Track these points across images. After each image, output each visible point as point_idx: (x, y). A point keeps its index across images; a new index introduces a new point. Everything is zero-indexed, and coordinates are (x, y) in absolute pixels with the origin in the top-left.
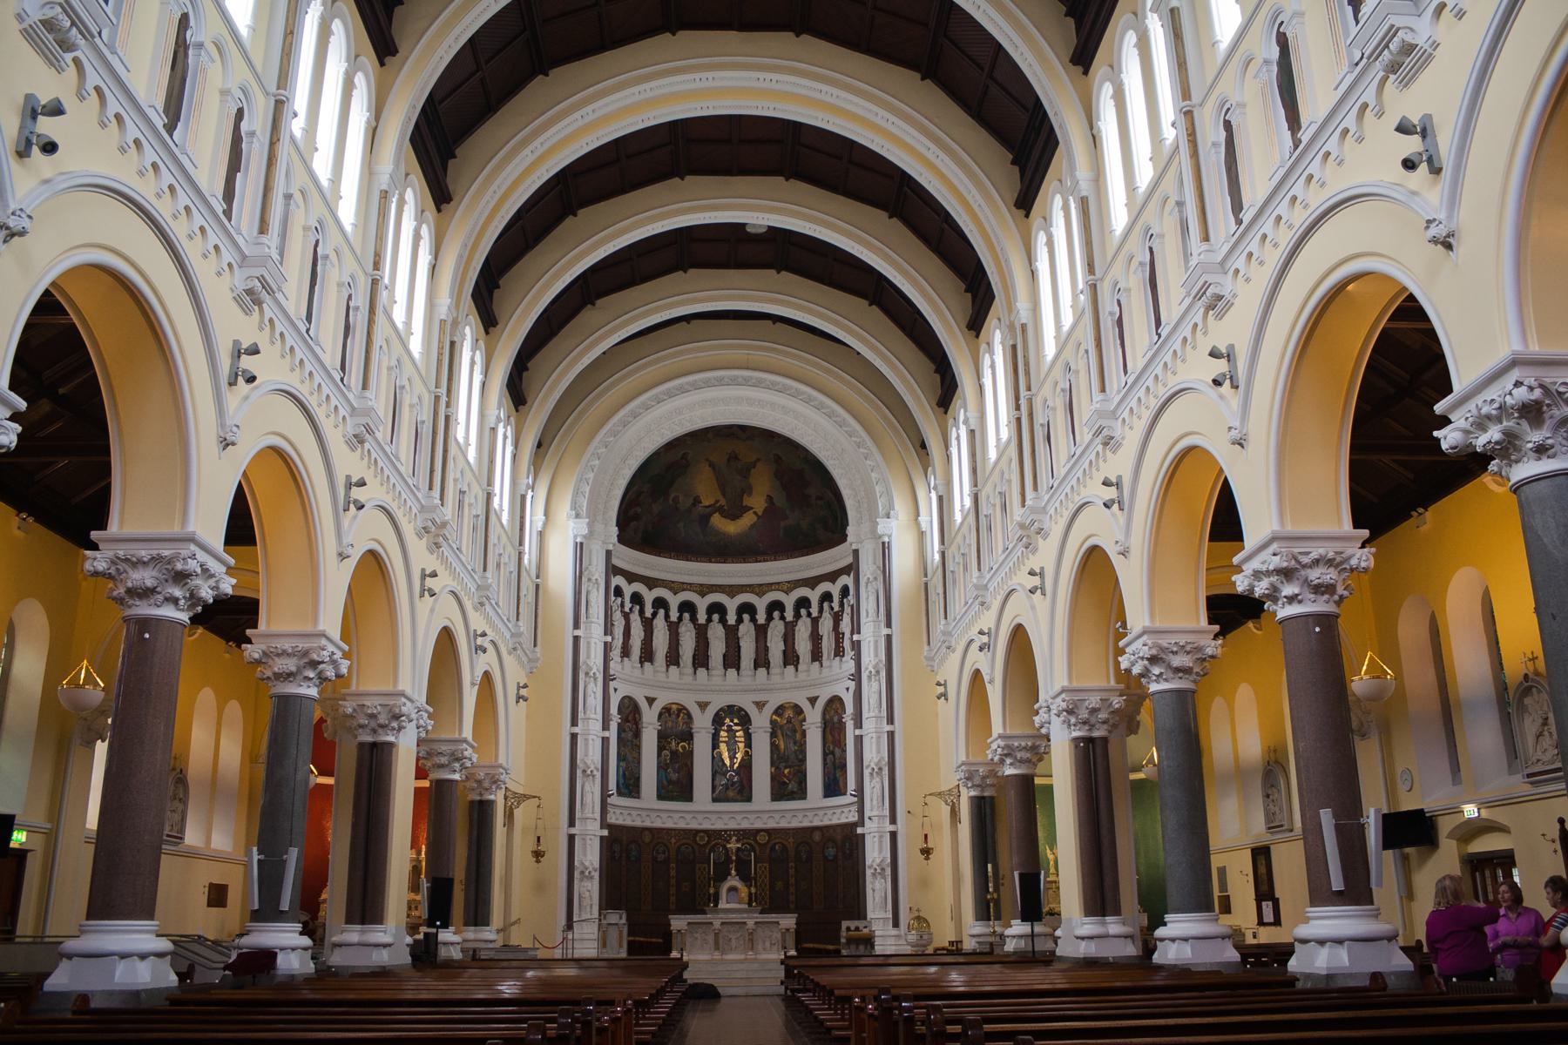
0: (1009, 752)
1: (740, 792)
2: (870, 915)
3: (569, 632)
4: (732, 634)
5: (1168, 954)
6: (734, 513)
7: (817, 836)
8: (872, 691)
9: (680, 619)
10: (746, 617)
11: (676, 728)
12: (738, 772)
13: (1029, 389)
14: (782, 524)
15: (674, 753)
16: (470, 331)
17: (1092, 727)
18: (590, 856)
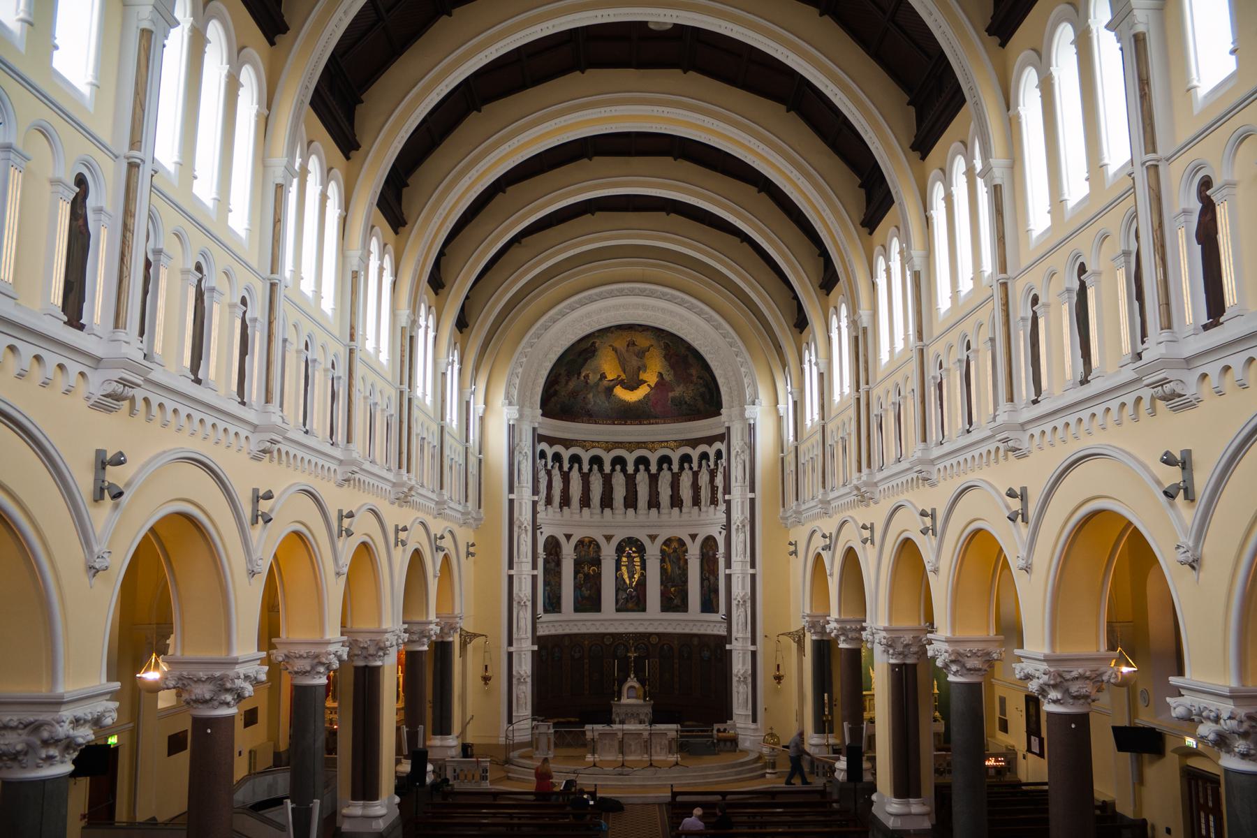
1: (637, 604)
3: (505, 496)
4: (631, 481)
6: (632, 387)
7: (696, 641)
9: (590, 470)
10: (642, 467)
11: (588, 555)
12: (636, 589)
13: (867, 383)
14: (671, 395)
15: (587, 576)
17: (905, 656)
18: (524, 667)
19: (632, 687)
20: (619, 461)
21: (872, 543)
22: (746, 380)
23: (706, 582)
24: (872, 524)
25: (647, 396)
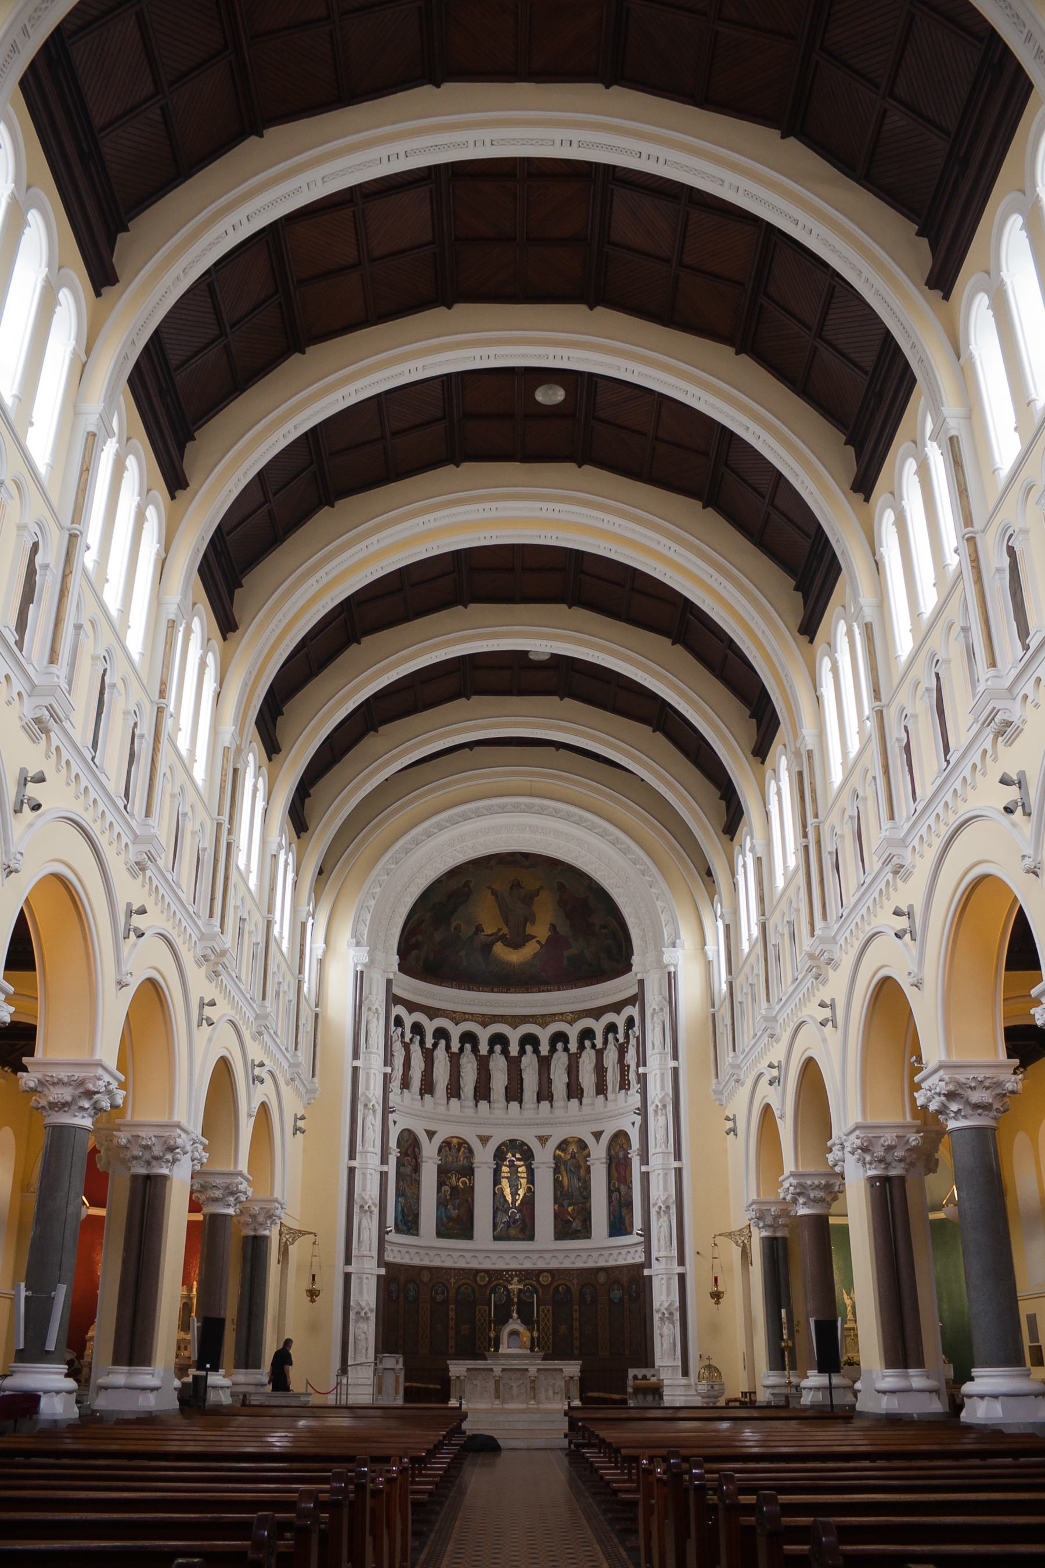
0: (801, 1191)
1: (522, 1230)
2: (658, 1363)
3: (348, 1063)
4: (514, 1067)
5: (978, 1412)
6: (517, 942)
7: (602, 1278)
8: (659, 1125)
9: (461, 1049)
10: (529, 1048)
12: (520, 1209)
13: (816, 816)
14: (566, 953)
15: (454, 1189)
16: (253, 758)
17: (888, 1165)
18: (366, 1296)
19: (514, 1333)
21: (835, 1026)
22: (663, 917)
23: (615, 1195)
24: (833, 1000)
25: (535, 955)
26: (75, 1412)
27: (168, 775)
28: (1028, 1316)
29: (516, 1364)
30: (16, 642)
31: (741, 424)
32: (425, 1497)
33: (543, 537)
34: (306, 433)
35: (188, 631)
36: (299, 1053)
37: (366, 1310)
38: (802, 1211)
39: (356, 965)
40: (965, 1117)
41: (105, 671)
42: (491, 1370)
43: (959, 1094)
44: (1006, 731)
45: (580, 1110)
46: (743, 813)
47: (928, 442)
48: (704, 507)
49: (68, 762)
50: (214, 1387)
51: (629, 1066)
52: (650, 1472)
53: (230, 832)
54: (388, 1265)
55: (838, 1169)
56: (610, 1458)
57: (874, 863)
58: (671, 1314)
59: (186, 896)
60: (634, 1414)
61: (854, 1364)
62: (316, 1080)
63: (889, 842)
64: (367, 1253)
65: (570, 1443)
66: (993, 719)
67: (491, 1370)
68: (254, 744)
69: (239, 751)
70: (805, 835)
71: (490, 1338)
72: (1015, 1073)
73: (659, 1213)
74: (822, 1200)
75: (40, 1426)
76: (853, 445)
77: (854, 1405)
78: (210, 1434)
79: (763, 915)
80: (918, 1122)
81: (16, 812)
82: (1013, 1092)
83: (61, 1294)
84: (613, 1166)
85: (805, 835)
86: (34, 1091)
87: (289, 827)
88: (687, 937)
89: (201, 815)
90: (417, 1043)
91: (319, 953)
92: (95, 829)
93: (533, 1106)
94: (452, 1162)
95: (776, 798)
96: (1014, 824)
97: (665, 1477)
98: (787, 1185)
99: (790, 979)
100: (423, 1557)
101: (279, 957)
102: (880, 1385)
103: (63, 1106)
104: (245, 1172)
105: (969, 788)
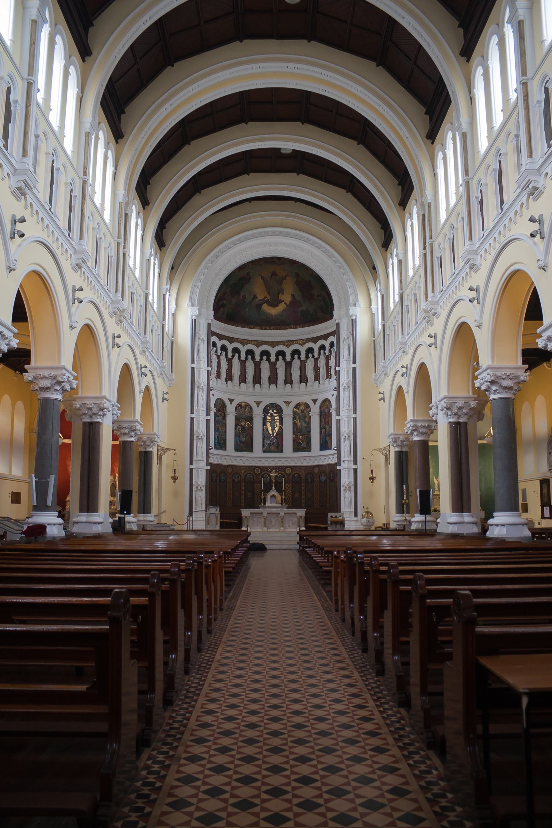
0: (416, 429)
1: (277, 447)
3: (189, 366)
5: (494, 532)
6: (274, 303)
7: (316, 470)
8: (346, 396)
9: (246, 358)
10: (280, 358)
11: (244, 415)
12: (276, 437)
13: (431, 238)
14: (299, 309)
15: (244, 428)
16: (135, 208)
18: (201, 479)
20: (265, 353)
21: (436, 347)
22: (350, 291)
23: (323, 430)
24: (436, 334)
25: (284, 310)
26: (63, 533)
27: (91, 217)
28: (522, 490)
29: (274, 510)
30: (4, 145)
31: (400, 15)
32: (231, 569)
33: (288, 83)
34: (156, 22)
35: (97, 139)
36: (164, 361)
37: (201, 486)
38: (416, 438)
39: (192, 316)
40: (499, 393)
41: (53, 161)
42: (262, 513)
43: (497, 382)
44: (534, 192)
45: (306, 388)
46: (392, 236)
47: (506, 24)
48: (377, 66)
49: (37, 211)
50: (129, 522)
51: (331, 367)
52: (337, 557)
53: (124, 247)
54: (211, 465)
55: (434, 418)
56: (319, 553)
57: (460, 263)
58: (350, 487)
59: (103, 281)
60: (331, 533)
61: (437, 511)
62: (173, 374)
63: (469, 252)
64: (201, 459)
65: (300, 546)
66: (528, 186)
67: (262, 513)
68: (135, 200)
69: (127, 204)
70: (425, 248)
71: (261, 499)
72: (525, 372)
73: (345, 439)
74: (425, 433)
75: (47, 540)
76: (462, 28)
77: (436, 530)
78: (128, 543)
79: (402, 290)
80: (475, 396)
81: (11, 238)
82: (524, 381)
83: (52, 479)
84: (323, 416)
85: (425, 248)
86: (31, 382)
87: (155, 244)
88: (362, 301)
89: (109, 238)
90: (224, 355)
91: (173, 310)
92: (54, 247)
93: (282, 387)
94: (242, 414)
95: (410, 228)
96: (535, 243)
97: (345, 559)
98: (409, 426)
99: (414, 323)
100: (230, 595)
101: (152, 312)
102: (449, 520)
103: (47, 389)
104: (139, 420)
105: (512, 223)
